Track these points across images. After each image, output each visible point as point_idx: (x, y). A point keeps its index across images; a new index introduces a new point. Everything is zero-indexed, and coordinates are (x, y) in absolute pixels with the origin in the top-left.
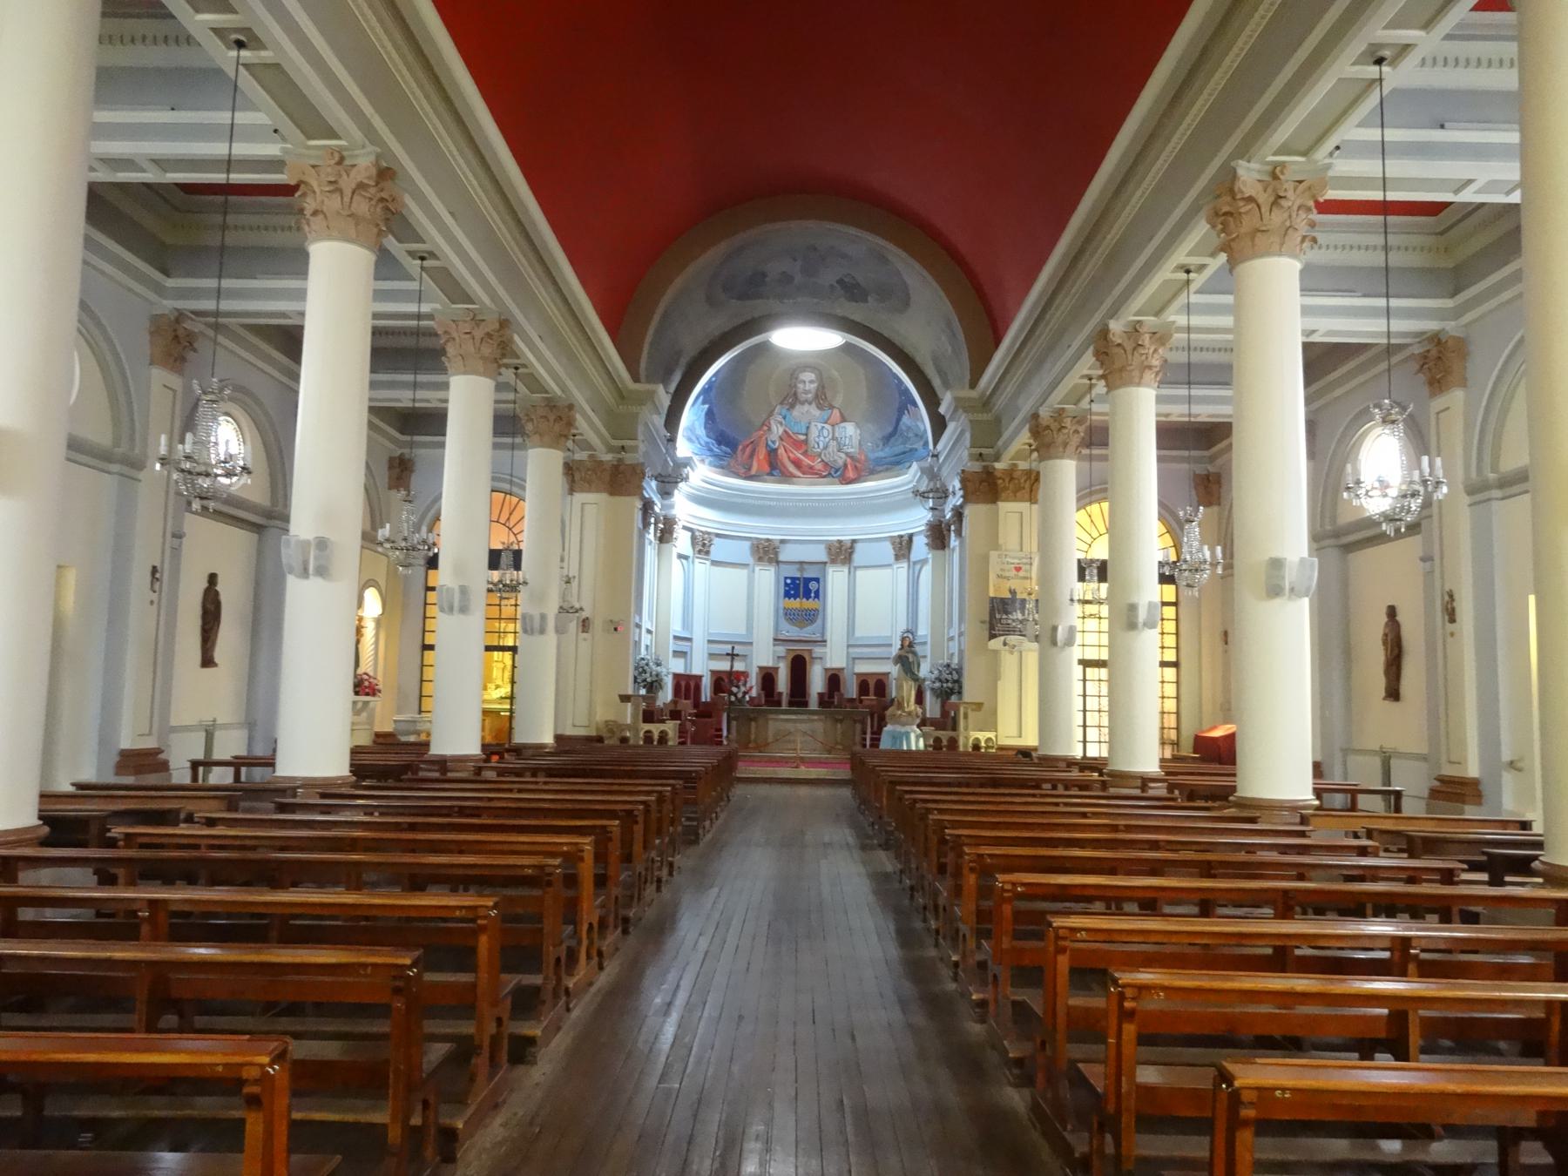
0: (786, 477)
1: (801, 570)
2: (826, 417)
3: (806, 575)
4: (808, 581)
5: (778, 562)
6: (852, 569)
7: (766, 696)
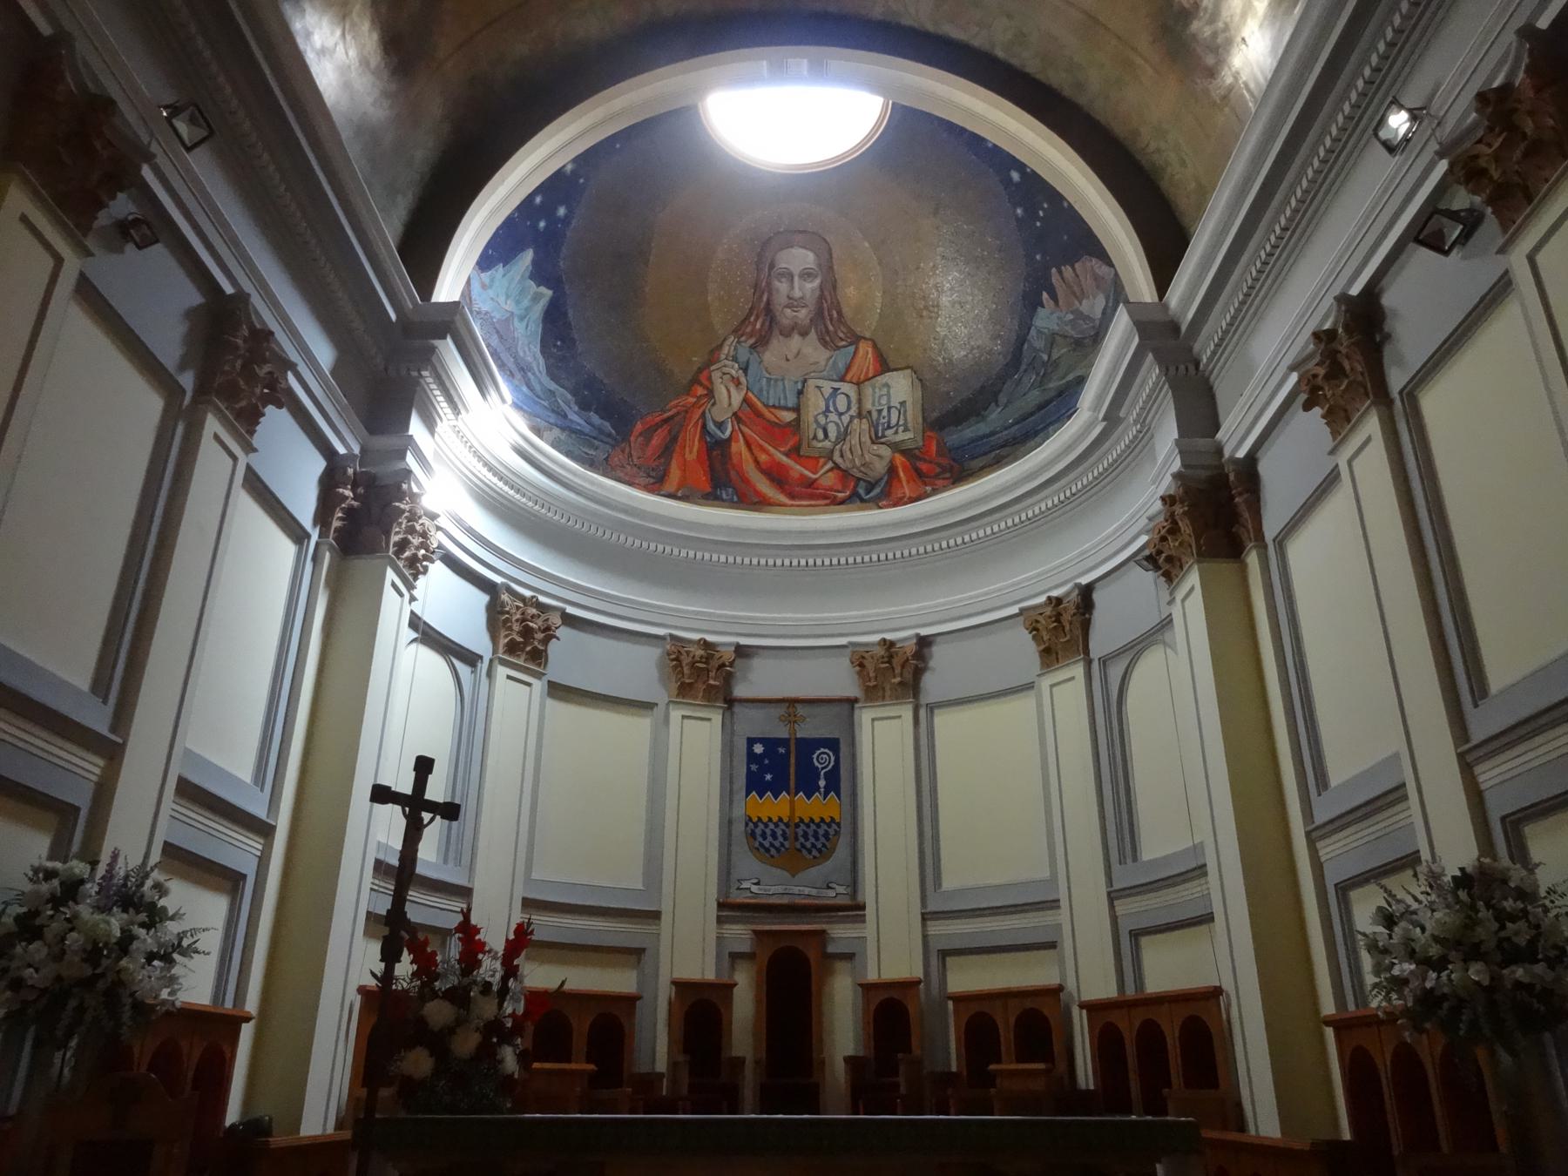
0: (749, 500)
1: (791, 719)
2: (841, 365)
3: (805, 731)
4: (808, 746)
5: (730, 702)
6: (922, 712)
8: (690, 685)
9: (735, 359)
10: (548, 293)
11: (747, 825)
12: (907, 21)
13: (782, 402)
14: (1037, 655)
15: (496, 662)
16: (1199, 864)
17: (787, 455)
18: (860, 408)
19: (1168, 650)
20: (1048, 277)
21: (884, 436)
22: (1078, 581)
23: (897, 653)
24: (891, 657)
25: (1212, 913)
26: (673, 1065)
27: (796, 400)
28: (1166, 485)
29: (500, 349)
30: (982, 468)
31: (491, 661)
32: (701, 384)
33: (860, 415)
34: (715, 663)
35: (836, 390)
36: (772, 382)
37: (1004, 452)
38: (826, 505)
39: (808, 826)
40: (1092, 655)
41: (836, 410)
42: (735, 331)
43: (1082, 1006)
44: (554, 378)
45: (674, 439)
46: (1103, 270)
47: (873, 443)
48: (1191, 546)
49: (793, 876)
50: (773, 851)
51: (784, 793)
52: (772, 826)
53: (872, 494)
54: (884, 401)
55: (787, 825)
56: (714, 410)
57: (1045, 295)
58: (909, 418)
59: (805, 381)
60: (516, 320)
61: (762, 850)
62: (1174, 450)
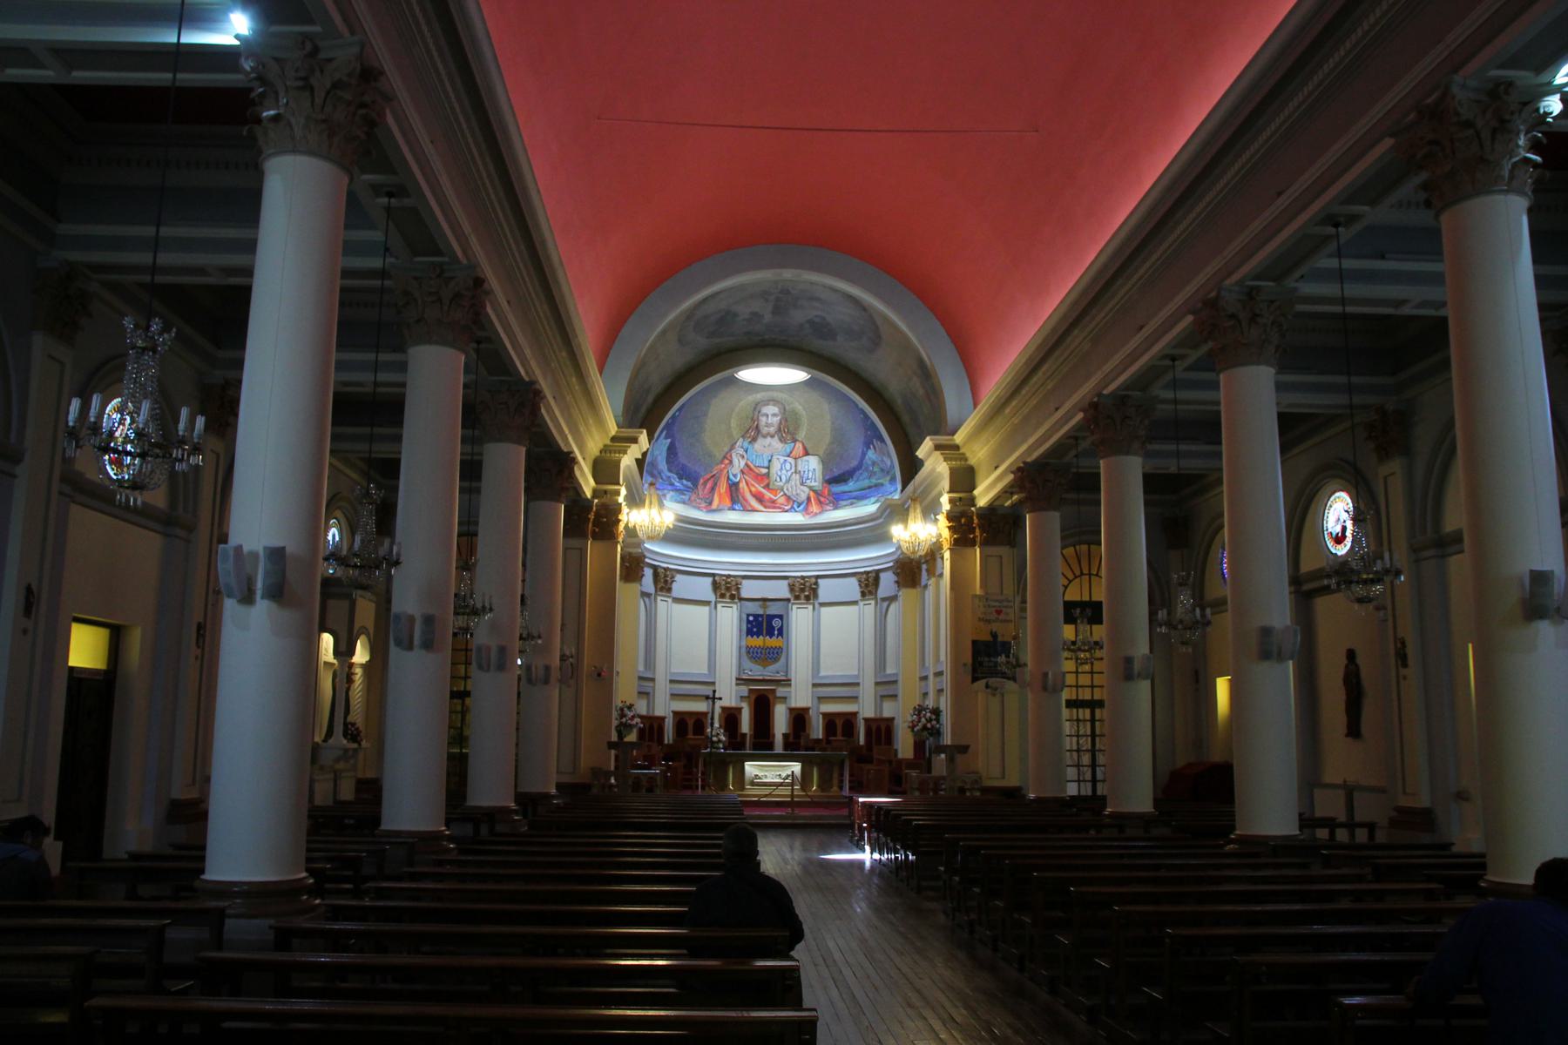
2: (788, 451)
4: (771, 617)
9: (742, 447)
17: (764, 488)
18: (796, 469)
32: (727, 459)
33: (796, 472)
37: (854, 501)
45: (716, 484)
58: (817, 475)
59: (772, 456)
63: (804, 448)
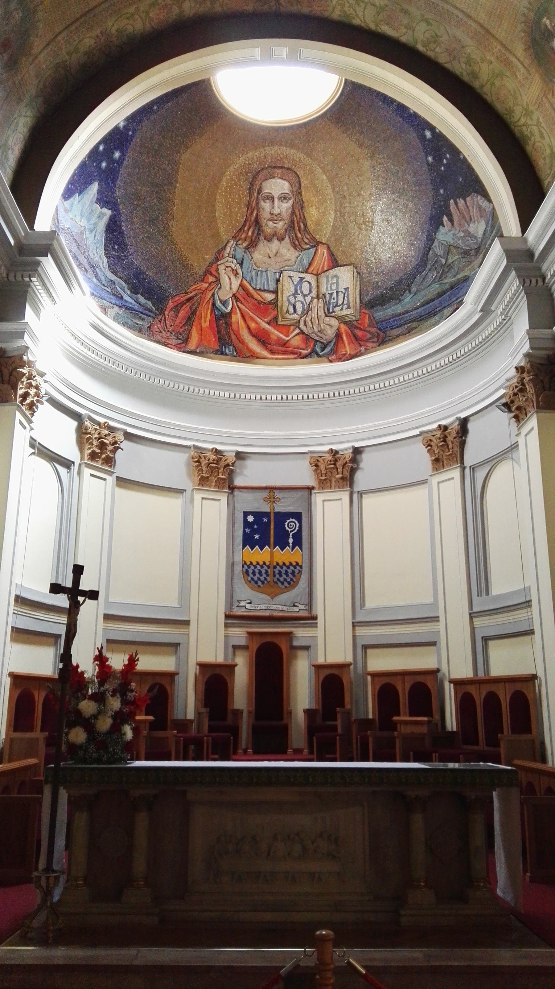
1: (272, 500)
2: (306, 262)
3: (280, 508)
4: (282, 517)
5: (232, 489)
6: (355, 496)
7: (211, 718)
8: (207, 478)
9: (234, 257)
10: (108, 212)
11: (243, 567)
12: (357, 22)
13: (266, 288)
14: (430, 463)
15: (83, 466)
16: (527, 600)
17: (269, 323)
19: (514, 463)
20: (447, 206)
21: (333, 312)
22: (458, 416)
23: (339, 459)
24: (336, 461)
25: (533, 629)
26: (198, 714)
27: (275, 286)
28: (519, 360)
29: (78, 253)
30: (398, 336)
31: (80, 465)
32: (211, 274)
33: (318, 297)
34: (223, 464)
35: (302, 279)
36: (259, 272)
37: (414, 325)
38: (295, 358)
39: (282, 568)
40: (465, 465)
41: (302, 293)
42: (234, 238)
43: (451, 681)
44: (115, 273)
45: (194, 313)
46: (485, 204)
47: (326, 316)
48: (533, 401)
49: (272, 598)
50: (260, 583)
51: (267, 547)
52: (259, 567)
53: (325, 352)
54: (334, 287)
55: (269, 567)
56: (220, 293)
57: (445, 218)
58: (351, 299)
59: (281, 272)
60: (87, 233)
61: (253, 582)
62: (525, 337)
63: (331, 254)
